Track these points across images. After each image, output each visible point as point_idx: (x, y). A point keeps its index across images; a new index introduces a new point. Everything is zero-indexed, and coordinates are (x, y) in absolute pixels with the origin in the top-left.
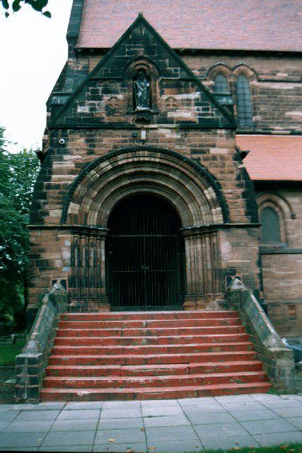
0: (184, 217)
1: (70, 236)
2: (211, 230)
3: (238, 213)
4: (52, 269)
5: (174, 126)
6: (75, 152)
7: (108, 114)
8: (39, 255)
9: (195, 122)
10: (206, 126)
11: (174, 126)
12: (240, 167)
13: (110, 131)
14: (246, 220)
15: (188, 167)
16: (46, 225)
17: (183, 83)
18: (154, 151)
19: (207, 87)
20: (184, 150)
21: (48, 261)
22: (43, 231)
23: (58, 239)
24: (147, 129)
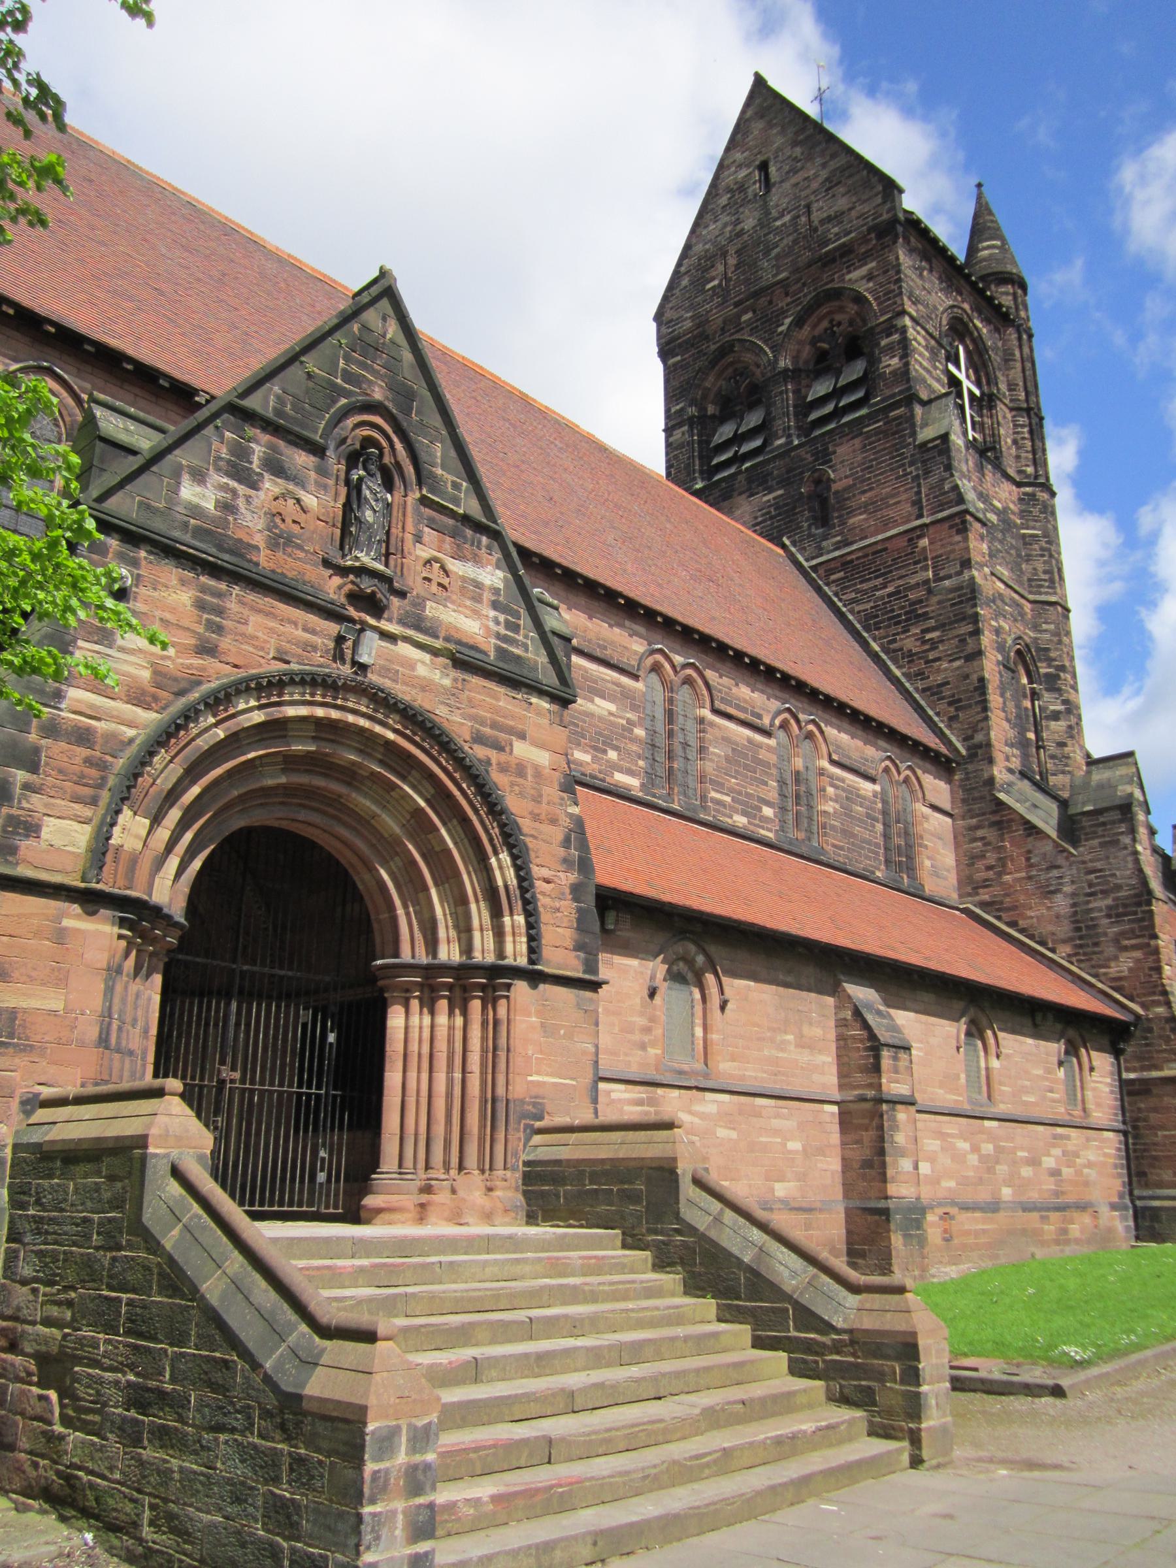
3: (560, 955)
9: (485, 653)
20: (456, 722)
23: (61, 936)
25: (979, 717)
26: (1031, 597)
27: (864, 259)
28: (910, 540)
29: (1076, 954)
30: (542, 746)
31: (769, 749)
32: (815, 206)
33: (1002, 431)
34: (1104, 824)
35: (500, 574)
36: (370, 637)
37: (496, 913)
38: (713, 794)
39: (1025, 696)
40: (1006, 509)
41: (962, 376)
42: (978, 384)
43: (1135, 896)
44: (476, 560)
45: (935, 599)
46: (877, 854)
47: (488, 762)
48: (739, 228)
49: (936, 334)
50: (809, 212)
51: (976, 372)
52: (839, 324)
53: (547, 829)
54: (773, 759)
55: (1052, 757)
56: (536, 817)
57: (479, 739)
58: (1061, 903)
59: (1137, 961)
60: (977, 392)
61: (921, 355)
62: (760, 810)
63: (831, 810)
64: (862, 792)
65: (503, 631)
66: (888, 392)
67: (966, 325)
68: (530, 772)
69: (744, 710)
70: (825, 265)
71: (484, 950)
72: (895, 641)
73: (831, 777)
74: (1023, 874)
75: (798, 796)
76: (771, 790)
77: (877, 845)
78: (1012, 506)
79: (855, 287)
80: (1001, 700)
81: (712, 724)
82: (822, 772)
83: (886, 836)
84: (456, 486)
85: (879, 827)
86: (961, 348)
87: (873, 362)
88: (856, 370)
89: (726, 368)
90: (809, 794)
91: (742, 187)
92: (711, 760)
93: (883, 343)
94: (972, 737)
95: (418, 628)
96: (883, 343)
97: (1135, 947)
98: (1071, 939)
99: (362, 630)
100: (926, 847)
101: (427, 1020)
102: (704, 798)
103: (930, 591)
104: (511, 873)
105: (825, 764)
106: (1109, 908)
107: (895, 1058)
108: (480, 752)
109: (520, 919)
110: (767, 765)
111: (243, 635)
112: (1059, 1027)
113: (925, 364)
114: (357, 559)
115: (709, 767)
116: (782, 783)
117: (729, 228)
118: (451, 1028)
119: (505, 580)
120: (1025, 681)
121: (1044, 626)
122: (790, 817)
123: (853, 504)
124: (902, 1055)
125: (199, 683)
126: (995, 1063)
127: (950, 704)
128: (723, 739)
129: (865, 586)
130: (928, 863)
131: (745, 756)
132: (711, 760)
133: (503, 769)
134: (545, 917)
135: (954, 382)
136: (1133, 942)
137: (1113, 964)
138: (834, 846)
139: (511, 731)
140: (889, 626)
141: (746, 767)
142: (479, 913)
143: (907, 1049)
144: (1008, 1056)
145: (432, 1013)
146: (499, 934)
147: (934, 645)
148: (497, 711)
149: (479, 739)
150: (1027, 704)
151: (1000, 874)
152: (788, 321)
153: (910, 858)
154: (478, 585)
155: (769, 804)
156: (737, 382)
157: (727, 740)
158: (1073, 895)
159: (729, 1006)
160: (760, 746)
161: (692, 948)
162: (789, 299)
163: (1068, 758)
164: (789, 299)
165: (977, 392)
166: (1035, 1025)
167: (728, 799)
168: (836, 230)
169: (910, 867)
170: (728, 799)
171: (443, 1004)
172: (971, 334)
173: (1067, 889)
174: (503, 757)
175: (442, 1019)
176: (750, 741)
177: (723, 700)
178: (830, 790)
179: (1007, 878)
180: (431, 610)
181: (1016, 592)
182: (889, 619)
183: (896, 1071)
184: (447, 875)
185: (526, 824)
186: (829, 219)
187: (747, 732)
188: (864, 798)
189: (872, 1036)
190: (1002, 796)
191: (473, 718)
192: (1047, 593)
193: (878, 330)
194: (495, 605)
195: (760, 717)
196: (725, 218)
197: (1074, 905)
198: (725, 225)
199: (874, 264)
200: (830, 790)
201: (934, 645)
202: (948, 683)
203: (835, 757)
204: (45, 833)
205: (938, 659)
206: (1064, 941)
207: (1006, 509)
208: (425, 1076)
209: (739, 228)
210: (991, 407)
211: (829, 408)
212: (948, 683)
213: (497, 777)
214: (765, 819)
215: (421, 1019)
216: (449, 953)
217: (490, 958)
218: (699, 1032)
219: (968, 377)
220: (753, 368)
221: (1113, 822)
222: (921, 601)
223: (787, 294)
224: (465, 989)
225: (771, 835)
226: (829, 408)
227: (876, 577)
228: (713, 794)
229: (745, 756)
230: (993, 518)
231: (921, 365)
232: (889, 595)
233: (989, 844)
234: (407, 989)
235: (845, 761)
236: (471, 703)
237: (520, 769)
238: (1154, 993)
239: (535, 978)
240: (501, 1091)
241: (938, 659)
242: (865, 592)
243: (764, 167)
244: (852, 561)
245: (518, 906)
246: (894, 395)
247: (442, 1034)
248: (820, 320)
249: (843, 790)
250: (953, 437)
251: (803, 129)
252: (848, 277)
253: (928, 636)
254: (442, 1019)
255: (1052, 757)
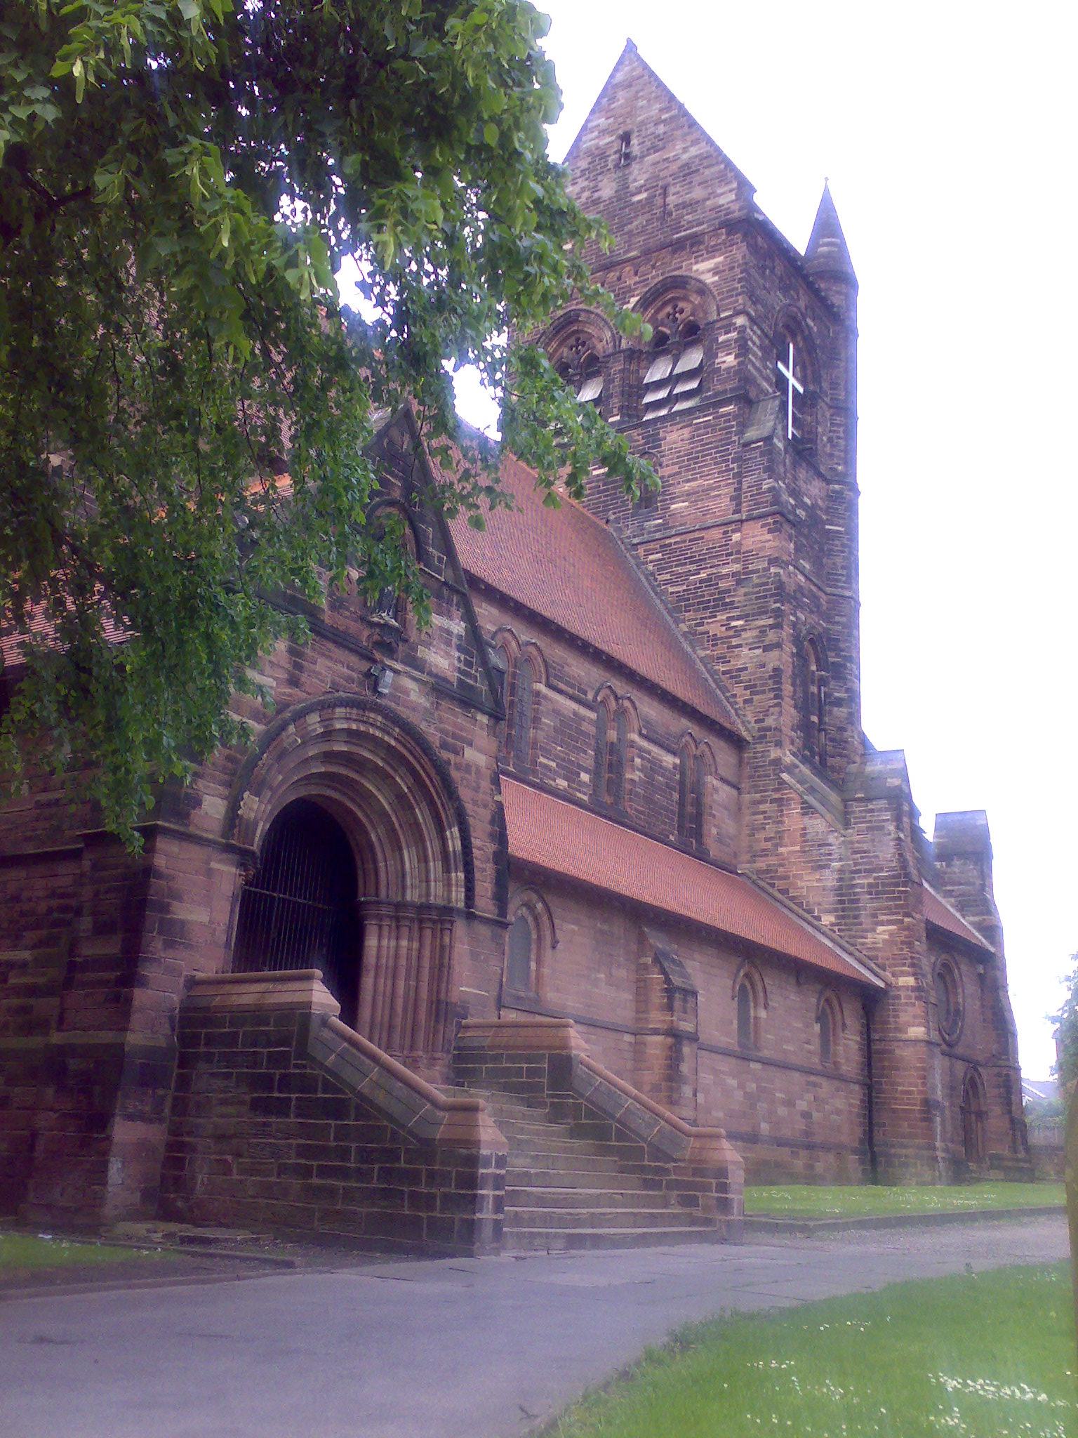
0: (385, 867)
1: (233, 870)
2: (435, 918)
3: (485, 904)
4: (189, 947)
5: (425, 677)
6: (268, 669)
7: (333, 607)
8: (169, 904)
9: (452, 684)
10: (465, 699)
11: (425, 677)
12: (496, 798)
13: (331, 646)
14: (729, 1039)
15: (433, 773)
16: (192, 829)
17: (445, 592)
18: (393, 722)
19: (1026, 1099)
20: (432, 734)
21: (183, 923)
22: (185, 845)
23: (210, 873)
24: (395, 672)
25: (772, 702)
26: (828, 590)
27: (712, 252)
28: (726, 533)
29: (838, 924)
30: (480, 751)
31: (591, 721)
32: (672, 190)
33: (820, 430)
34: (872, 811)
35: (463, 624)
36: (389, 674)
37: (447, 870)
38: (542, 759)
39: (813, 683)
40: (815, 506)
41: (789, 374)
42: (803, 382)
43: (894, 877)
44: (450, 618)
45: (742, 591)
46: (673, 820)
47: (449, 763)
48: (596, 195)
49: (771, 334)
50: (665, 194)
51: (804, 368)
52: (682, 311)
53: (481, 811)
54: (592, 730)
55: (832, 740)
56: (475, 803)
57: (444, 745)
58: (829, 879)
59: (891, 935)
60: (801, 390)
61: (755, 355)
62: (579, 775)
63: (637, 779)
64: (664, 764)
65: (463, 667)
66: (720, 388)
67: (798, 324)
68: (473, 769)
69: (572, 686)
70: (674, 252)
71: (437, 893)
72: (702, 624)
73: (641, 749)
74: (798, 848)
75: (610, 765)
76: (588, 759)
77: (673, 812)
78: (820, 502)
79: (703, 277)
80: (791, 689)
81: (545, 697)
82: (632, 744)
83: (681, 803)
84: (440, 560)
85: (676, 796)
86: (791, 346)
87: (710, 355)
88: (693, 359)
89: (568, 337)
90: (620, 762)
91: (603, 156)
92: (542, 729)
93: (721, 339)
94: (762, 721)
95: (416, 668)
96: (721, 339)
97: (890, 923)
98: (836, 910)
99: (383, 669)
100: (714, 816)
101: (393, 943)
102: (534, 762)
103: (739, 582)
104: (458, 843)
105: (635, 737)
106: (870, 885)
107: (685, 1001)
108: (445, 755)
109: (461, 875)
110: (587, 735)
111: (314, 672)
112: (819, 987)
113: (758, 364)
114: (382, 618)
115: (541, 735)
116: (598, 751)
117: (586, 194)
118: (410, 949)
119: (466, 629)
120: (814, 668)
121: (837, 619)
122: (604, 783)
123: (677, 490)
124: (690, 998)
125: (288, 705)
126: (763, 1014)
127: (746, 688)
128: (554, 711)
129: (680, 570)
130: (714, 831)
131: (570, 727)
132: (542, 729)
133: (458, 767)
134: (477, 875)
135: (781, 382)
136: (888, 917)
137: (869, 935)
138: (636, 810)
139: (463, 740)
140: (698, 610)
141: (571, 737)
142: (435, 867)
143: (694, 994)
144: (774, 1008)
145: (398, 939)
146: (448, 885)
147: (738, 632)
148: (455, 725)
149: (444, 745)
150: (814, 689)
151: (777, 846)
152: (634, 300)
153: (700, 826)
154: (449, 632)
155: (587, 771)
156: (578, 352)
157: (556, 712)
158: (841, 871)
159: (559, 946)
160: (583, 719)
161: (534, 897)
162: (637, 279)
163: (846, 742)
164: (637, 279)
165: (801, 390)
166: (798, 983)
167: (553, 764)
168: (689, 217)
169: (698, 834)
170: (553, 764)
171: (405, 931)
172: (803, 332)
173: (835, 865)
174: (458, 759)
175: (404, 943)
176: (575, 713)
177: (556, 676)
178: (638, 761)
179: (781, 850)
180: (422, 652)
181: (815, 585)
182: (699, 603)
183: (685, 1012)
184: (420, 840)
185: (469, 807)
186: (684, 205)
187: (574, 706)
188: (665, 769)
189: (668, 981)
190: (785, 776)
191: (441, 731)
192: (842, 588)
193: (718, 325)
194: (459, 648)
195: (585, 693)
196: (582, 183)
197: (840, 880)
198: (583, 189)
199: (721, 259)
200: (638, 761)
201: (738, 632)
202: (746, 669)
203: (644, 732)
204: (205, 804)
205: (740, 646)
206: (828, 911)
207: (815, 506)
208: (389, 983)
209: (596, 195)
210: (813, 406)
211: (662, 394)
212: (746, 669)
213: (455, 774)
214: (581, 783)
215: (379, 940)
216: (412, 896)
217: (440, 902)
218: (533, 965)
219: (794, 375)
220: (595, 341)
221: (880, 810)
222: (729, 591)
223: (636, 274)
224: (421, 921)
225: (585, 798)
226: (662, 394)
227: (691, 563)
228: (542, 759)
229: (570, 727)
230: (801, 513)
231: (754, 365)
232: (701, 582)
233: (769, 818)
234: (380, 918)
235: (651, 735)
236: (441, 720)
237: (468, 768)
238: (904, 965)
239: (470, 917)
240: (443, 996)
241: (740, 646)
242: (679, 575)
243: (626, 138)
244: (670, 545)
245: (461, 867)
246: (725, 391)
247: (404, 951)
248: (665, 304)
249: (649, 761)
250: (775, 440)
251: (668, 109)
252: (695, 268)
253: (733, 624)
254: (404, 943)
255: (832, 740)
